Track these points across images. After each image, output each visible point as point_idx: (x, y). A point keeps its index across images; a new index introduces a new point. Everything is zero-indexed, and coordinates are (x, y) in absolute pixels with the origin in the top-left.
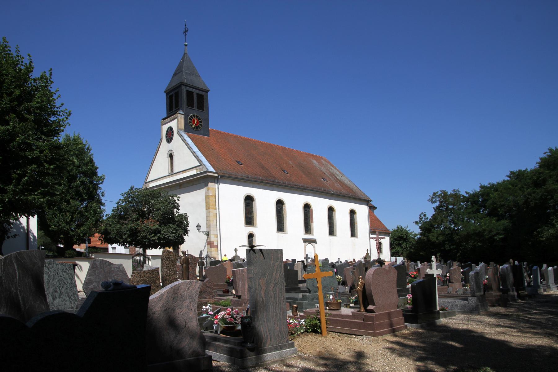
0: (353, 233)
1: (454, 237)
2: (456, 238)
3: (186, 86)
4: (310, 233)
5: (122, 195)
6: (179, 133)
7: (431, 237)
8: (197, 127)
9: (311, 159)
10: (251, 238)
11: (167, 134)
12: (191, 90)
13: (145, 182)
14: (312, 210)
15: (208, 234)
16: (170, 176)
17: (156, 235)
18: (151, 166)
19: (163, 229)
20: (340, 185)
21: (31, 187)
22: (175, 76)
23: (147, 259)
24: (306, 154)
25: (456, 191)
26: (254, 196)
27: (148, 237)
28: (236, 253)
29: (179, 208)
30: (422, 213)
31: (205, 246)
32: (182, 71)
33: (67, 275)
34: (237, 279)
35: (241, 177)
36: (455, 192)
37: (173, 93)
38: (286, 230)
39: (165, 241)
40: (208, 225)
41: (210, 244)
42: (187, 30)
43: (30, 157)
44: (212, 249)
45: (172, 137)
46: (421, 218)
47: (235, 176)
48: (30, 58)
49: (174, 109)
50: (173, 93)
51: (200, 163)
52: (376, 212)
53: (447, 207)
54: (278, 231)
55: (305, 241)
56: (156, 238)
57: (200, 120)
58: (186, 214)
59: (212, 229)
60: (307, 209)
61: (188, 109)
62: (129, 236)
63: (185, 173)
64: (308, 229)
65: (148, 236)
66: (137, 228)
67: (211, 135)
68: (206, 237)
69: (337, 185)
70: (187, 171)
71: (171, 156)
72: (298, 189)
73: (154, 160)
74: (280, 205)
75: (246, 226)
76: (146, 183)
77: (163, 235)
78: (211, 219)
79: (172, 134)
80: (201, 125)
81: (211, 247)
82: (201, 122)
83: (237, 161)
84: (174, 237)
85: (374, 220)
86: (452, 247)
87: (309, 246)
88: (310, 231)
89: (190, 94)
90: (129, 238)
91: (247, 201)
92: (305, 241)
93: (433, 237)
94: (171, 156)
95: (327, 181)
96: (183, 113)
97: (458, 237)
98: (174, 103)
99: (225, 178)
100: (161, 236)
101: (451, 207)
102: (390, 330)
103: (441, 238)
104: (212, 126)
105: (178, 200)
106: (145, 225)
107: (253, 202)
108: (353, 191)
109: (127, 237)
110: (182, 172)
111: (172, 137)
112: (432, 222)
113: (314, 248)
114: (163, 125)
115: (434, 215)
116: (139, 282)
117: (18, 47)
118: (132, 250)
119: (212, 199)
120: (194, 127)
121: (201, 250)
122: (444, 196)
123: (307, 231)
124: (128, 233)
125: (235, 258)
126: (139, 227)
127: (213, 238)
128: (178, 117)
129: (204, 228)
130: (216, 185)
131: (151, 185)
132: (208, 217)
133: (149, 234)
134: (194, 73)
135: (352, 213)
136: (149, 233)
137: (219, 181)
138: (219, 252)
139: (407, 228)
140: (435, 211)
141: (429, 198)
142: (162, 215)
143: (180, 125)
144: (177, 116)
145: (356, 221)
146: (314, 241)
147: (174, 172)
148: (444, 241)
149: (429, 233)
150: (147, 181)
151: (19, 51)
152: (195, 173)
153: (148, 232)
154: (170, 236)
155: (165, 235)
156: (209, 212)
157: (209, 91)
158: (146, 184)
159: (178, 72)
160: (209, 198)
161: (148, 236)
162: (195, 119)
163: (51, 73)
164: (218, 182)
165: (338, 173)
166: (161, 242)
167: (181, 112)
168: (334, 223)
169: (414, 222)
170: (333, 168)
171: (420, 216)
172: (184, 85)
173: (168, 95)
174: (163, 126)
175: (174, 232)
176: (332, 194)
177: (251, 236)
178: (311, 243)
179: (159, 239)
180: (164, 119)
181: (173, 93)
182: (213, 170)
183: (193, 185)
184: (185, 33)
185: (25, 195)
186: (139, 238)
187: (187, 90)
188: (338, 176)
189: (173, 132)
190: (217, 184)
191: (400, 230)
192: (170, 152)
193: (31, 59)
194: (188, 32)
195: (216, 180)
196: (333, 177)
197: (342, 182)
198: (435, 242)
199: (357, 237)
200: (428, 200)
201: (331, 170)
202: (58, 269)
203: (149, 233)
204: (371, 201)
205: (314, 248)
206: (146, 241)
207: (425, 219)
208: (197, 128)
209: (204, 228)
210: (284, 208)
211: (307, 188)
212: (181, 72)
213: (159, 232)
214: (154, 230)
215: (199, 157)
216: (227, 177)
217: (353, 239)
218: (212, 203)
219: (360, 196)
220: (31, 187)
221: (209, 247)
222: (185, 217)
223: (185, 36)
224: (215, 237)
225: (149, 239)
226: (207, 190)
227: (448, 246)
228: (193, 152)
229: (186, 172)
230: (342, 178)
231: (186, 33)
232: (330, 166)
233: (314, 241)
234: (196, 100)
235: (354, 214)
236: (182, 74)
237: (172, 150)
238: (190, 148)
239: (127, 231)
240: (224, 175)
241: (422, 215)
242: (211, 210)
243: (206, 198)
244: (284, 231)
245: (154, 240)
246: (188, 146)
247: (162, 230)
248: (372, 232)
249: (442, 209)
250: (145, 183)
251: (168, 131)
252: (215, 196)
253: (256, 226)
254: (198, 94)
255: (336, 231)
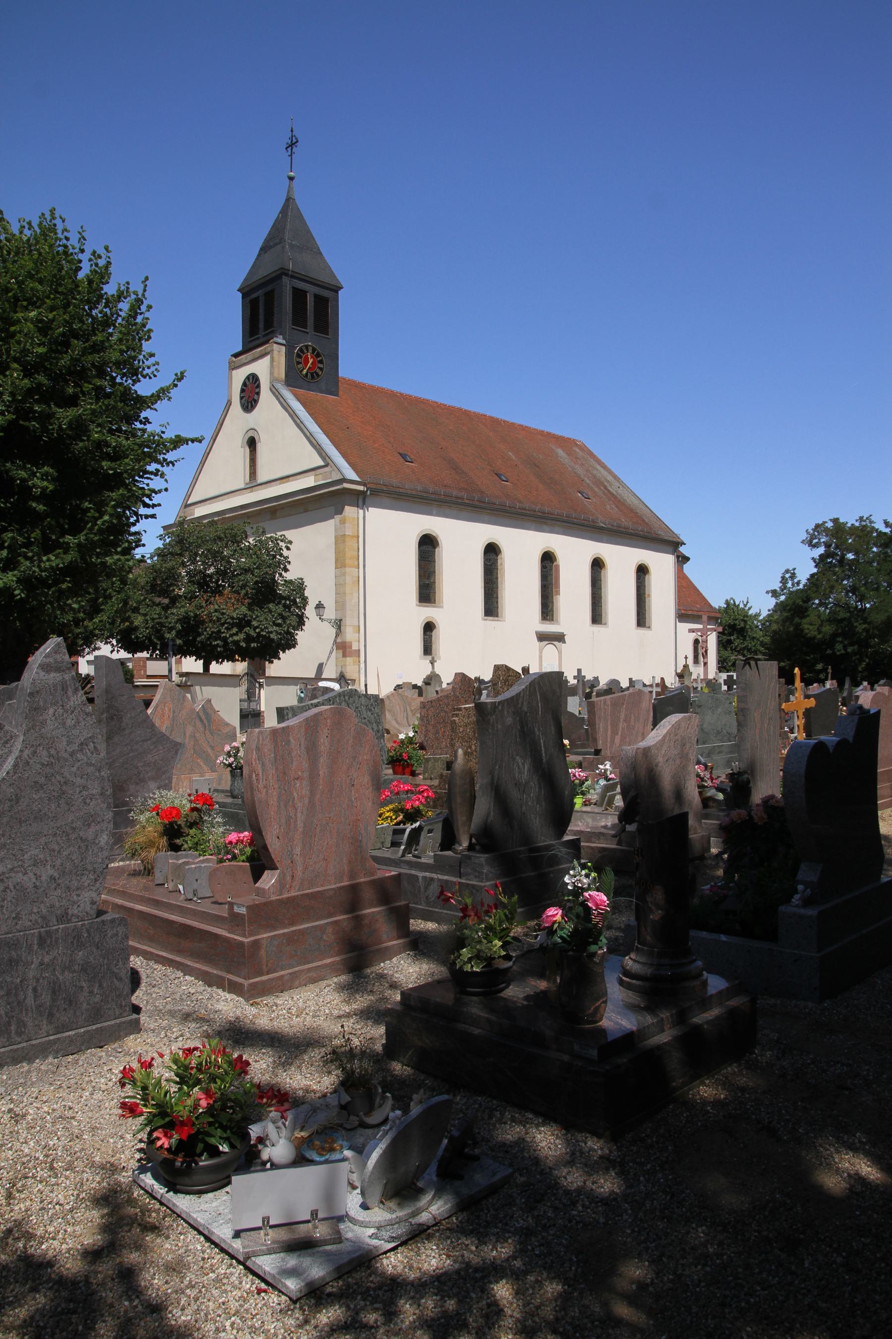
0: (642, 620)
1: (856, 627)
2: (860, 627)
3: (292, 277)
4: (553, 620)
5: (161, 539)
6: (274, 390)
7: (806, 626)
8: (312, 374)
9: (553, 447)
10: (428, 633)
11: (242, 391)
12: (302, 285)
13: (184, 504)
14: (558, 567)
15: (339, 625)
16: (248, 490)
17: (240, 631)
18: (201, 465)
19: (257, 617)
20: (617, 507)
21: (112, 538)
22: (266, 252)
23: (257, 685)
24: (542, 435)
25: (865, 521)
26: (438, 536)
27: (224, 635)
28: (433, 668)
29: (288, 567)
30: (787, 571)
31: (331, 653)
32: (282, 241)
33: (372, 717)
34: (597, 718)
35: (414, 492)
36: (864, 523)
37: (260, 291)
38: (502, 613)
39: (261, 643)
40: (340, 604)
41: (343, 648)
42: (294, 140)
43: (111, 472)
44: (348, 659)
45: (256, 397)
46: (784, 580)
47: (401, 490)
48: (109, 254)
49: (262, 332)
50: (260, 293)
51: (323, 459)
52: (687, 568)
53: (843, 556)
54: (485, 616)
55: (543, 637)
56: (242, 636)
57: (320, 358)
58: (302, 579)
59: (348, 613)
60: (547, 564)
61: (295, 331)
62: (179, 634)
63: (287, 482)
64: (547, 611)
65: (224, 632)
66: (200, 614)
67: (341, 393)
68: (333, 631)
69: (610, 507)
70: (290, 478)
71: (252, 443)
72: (531, 518)
73: (208, 451)
74: (492, 556)
75: (419, 606)
76: (187, 506)
77: (257, 630)
78: (348, 590)
79: (257, 390)
80: (321, 369)
81: (344, 655)
82: (321, 362)
83: (400, 454)
84: (280, 634)
85: (684, 588)
86: (850, 650)
87: (550, 649)
88: (553, 616)
89: (299, 296)
90: (180, 639)
91: (424, 548)
92: (543, 637)
93: (811, 627)
94: (252, 443)
95: (589, 499)
96: (284, 342)
97: (864, 626)
98: (261, 317)
99: (381, 494)
100: (252, 633)
101: (850, 556)
102: (561, 865)
103: (828, 629)
104: (346, 370)
105: (288, 549)
106: (216, 607)
107: (435, 548)
108: (644, 521)
109: (176, 636)
110: (278, 482)
111: (256, 397)
112: (809, 591)
113: (560, 653)
114: (233, 369)
115: (812, 576)
116: (466, 726)
117: (83, 231)
118: (140, 666)
119: (350, 543)
120: (307, 374)
121: (322, 662)
122: (838, 530)
123: (545, 615)
124: (179, 626)
125: (431, 680)
126: (203, 612)
127: (349, 635)
128: (272, 350)
129: (330, 613)
130: (361, 511)
131: (199, 512)
132: (340, 586)
133: (226, 628)
134: (309, 245)
135: (642, 571)
136: (226, 625)
137: (368, 501)
138: (362, 665)
139: (745, 606)
140: (816, 566)
141: (804, 536)
142: (256, 583)
143: (276, 371)
144: (269, 349)
145: (649, 591)
146: (559, 638)
147: (259, 481)
148: (834, 635)
149: (801, 618)
150: (189, 502)
151: (85, 240)
152: (312, 484)
153: (223, 625)
154: (271, 632)
155: (262, 630)
156: (344, 574)
157: (342, 288)
158: (188, 509)
159: (272, 244)
160: (344, 542)
161: (224, 632)
162: (309, 357)
163: (146, 286)
164: (364, 503)
165: (610, 478)
166: (252, 645)
167: (280, 339)
168: (603, 595)
169: (767, 592)
170: (598, 467)
171: (783, 578)
172: (287, 275)
173: (249, 299)
174: (234, 372)
175: (280, 621)
176: (602, 529)
177: (429, 627)
178: (554, 643)
179: (249, 639)
180: (236, 355)
181: (260, 293)
182: (356, 478)
183: (306, 511)
184: (289, 149)
185: (98, 555)
186: (203, 637)
187: (293, 288)
188: (611, 485)
189: (259, 386)
190: (362, 509)
191: (730, 606)
192: (250, 434)
193: (109, 258)
194: (287, 144)
195: (360, 499)
196: (600, 488)
197: (620, 501)
198: (814, 638)
199: (649, 627)
200: (803, 542)
201: (595, 472)
202: (361, 705)
203: (226, 625)
204: (683, 544)
205: (560, 653)
206: (218, 644)
207: (793, 585)
208: (313, 377)
209: (330, 613)
210: (499, 562)
211: (550, 516)
212: (280, 243)
213: (248, 624)
214: (238, 618)
215: (323, 446)
216: (383, 491)
217: (642, 631)
218: (349, 553)
219: (660, 532)
220: (112, 538)
221: (341, 655)
222: (299, 587)
223: (291, 155)
224: (354, 632)
225: (225, 640)
226: (341, 524)
227: (841, 646)
228: (308, 434)
229: (289, 481)
230: (620, 491)
231: (292, 149)
232: (592, 462)
233: (559, 638)
234: (313, 309)
235: (645, 575)
236: (283, 247)
237: (256, 428)
238: (302, 425)
239: (176, 623)
240: (378, 487)
241: (787, 576)
242: (348, 570)
243: (336, 541)
244: (497, 616)
245: (236, 643)
246: (296, 419)
247: (254, 619)
248: (683, 616)
249: (832, 561)
250: (183, 506)
251: (248, 383)
252: (358, 537)
253: (441, 605)
254: (317, 297)
255: (605, 613)
